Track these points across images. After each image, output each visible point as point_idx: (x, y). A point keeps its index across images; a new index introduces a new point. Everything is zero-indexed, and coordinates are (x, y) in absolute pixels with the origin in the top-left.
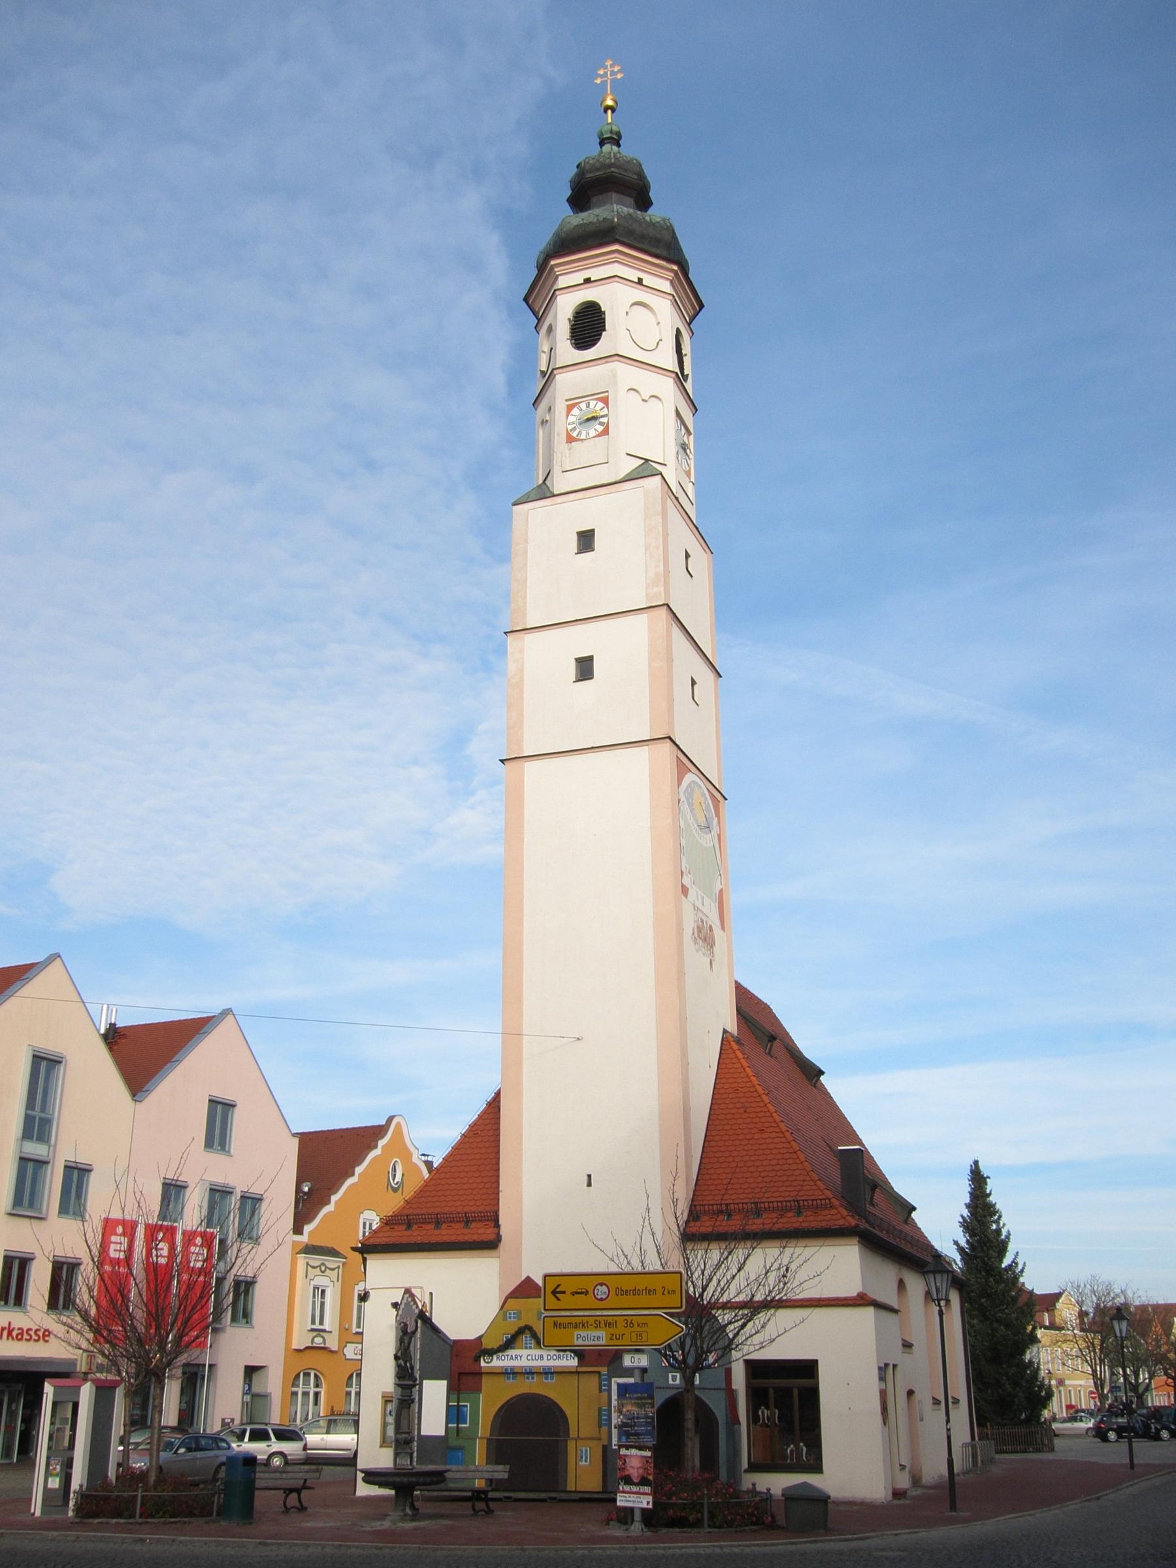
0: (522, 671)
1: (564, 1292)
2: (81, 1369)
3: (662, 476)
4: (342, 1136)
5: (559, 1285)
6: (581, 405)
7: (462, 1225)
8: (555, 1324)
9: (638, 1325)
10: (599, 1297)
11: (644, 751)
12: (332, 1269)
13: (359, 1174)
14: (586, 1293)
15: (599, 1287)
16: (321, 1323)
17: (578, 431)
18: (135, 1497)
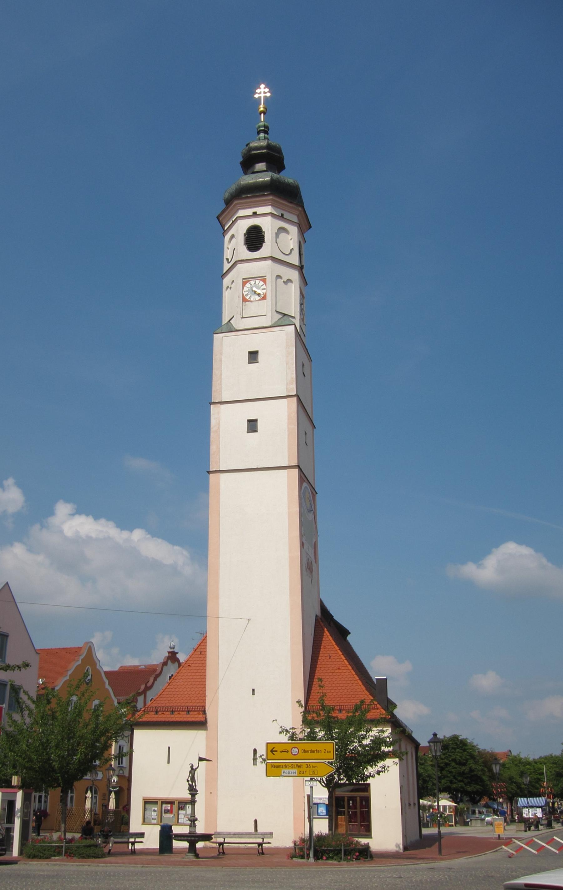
0: (219, 424)
1: (276, 751)
2: (14, 784)
3: (295, 326)
4: (57, 653)
5: (274, 748)
6: (251, 282)
7: (154, 713)
8: (272, 766)
9: (313, 767)
10: (294, 754)
11: (285, 472)
12: (126, 737)
13: (70, 675)
14: (287, 752)
15: (293, 749)
16: (122, 764)
17: (249, 296)
18: (62, 846)
